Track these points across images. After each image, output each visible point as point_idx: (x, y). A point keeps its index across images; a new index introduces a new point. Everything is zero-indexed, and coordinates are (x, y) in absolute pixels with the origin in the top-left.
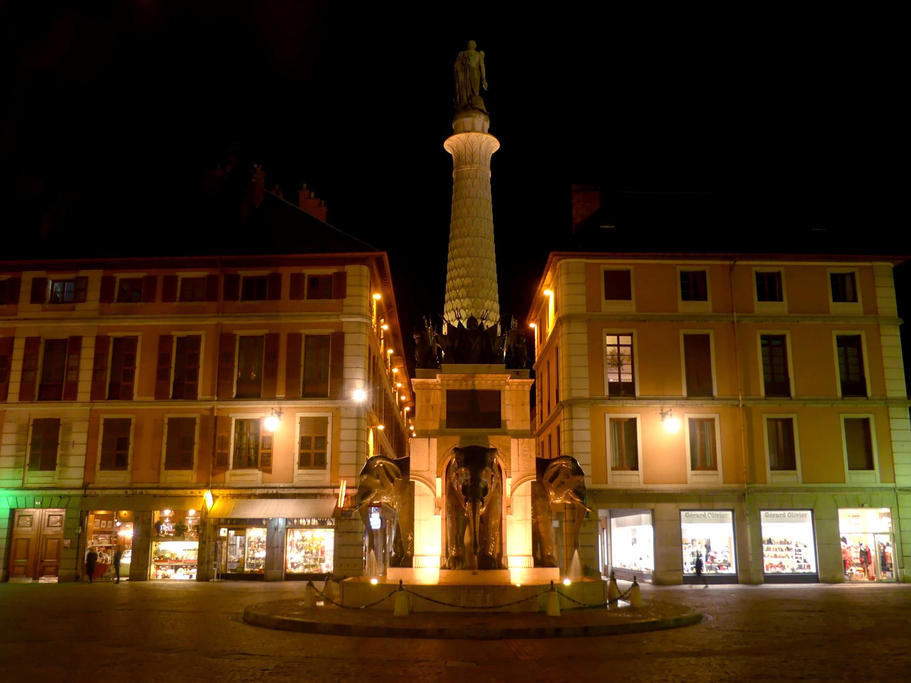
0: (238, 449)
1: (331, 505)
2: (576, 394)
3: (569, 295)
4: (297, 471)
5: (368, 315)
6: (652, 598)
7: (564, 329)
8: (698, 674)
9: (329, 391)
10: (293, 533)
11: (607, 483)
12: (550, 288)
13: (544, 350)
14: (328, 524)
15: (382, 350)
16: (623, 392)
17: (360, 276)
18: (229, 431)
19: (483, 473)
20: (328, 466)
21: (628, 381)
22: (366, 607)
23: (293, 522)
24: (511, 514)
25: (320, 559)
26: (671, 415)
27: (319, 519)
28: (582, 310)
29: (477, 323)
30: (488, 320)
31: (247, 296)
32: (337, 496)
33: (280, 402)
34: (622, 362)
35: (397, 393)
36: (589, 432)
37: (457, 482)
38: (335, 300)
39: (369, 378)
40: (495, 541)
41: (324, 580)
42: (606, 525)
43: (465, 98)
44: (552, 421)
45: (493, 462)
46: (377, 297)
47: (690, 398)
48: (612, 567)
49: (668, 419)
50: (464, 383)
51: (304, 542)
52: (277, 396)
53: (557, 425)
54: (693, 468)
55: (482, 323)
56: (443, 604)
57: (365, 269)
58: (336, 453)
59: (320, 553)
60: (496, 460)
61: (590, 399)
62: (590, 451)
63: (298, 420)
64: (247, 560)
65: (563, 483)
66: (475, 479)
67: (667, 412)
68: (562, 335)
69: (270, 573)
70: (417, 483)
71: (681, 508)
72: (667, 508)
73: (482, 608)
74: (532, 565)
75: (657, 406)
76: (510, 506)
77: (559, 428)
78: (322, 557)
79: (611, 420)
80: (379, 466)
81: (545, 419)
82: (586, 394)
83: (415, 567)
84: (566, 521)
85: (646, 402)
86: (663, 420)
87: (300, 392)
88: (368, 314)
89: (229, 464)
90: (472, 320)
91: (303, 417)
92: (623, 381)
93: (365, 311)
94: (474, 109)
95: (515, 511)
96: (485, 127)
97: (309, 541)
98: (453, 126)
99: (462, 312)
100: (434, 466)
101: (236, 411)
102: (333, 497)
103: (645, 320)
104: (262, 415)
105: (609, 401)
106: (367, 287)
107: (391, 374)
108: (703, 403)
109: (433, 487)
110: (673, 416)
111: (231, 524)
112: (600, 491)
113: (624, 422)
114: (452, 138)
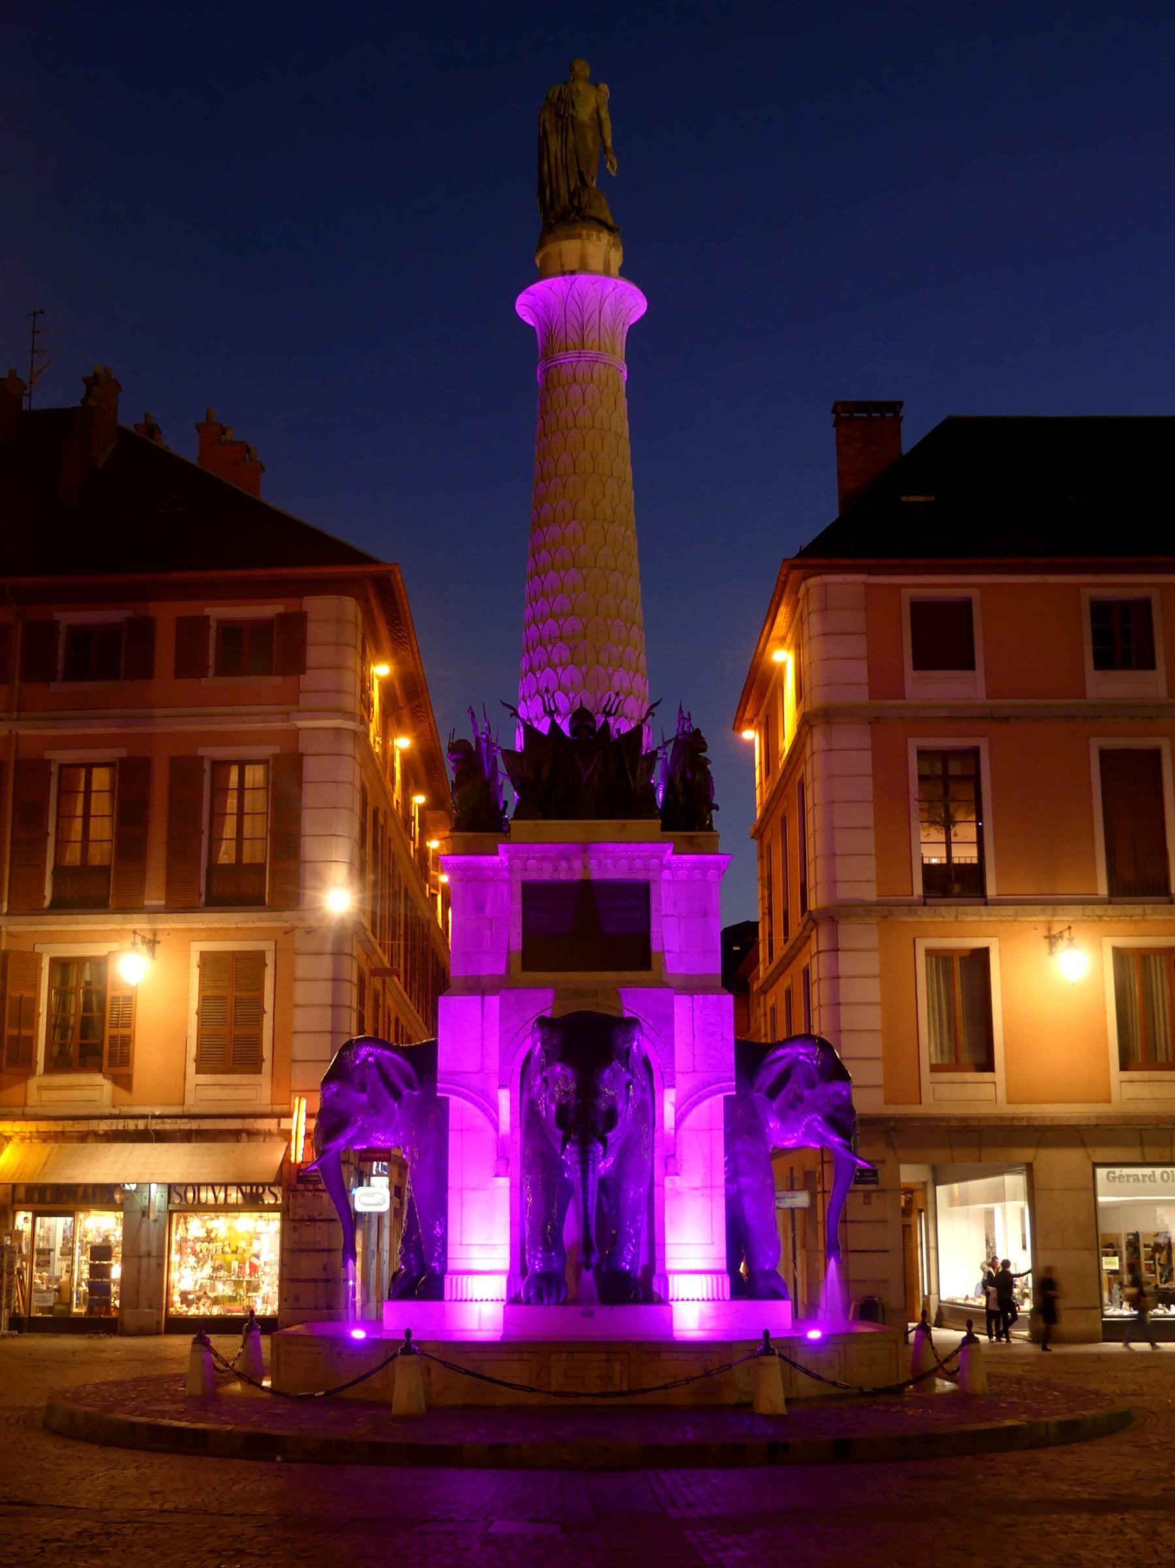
0: (58, 1025)
1: (269, 1158)
2: (845, 892)
3: (828, 659)
4: (194, 1079)
5: (358, 711)
6: (1020, 1372)
7: (817, 741)
8: (1083, 1553)
9: (267, 891)
10: (185, 1223)
11: (921, 1103)
12: (786, 646)
13: (775, 793)
14: (266, 1202)
15: (397, 795)
16: (957, 888)
17: (340, 621)
18: (36, 987)
19: (606, 1076)
20: (267, 1066)
21: (968, 861)
22: (327, 1393)
23: (184, 1197)
24: (677, 1174)
25: (249, 1282)
26: (1071, 940)
27: (243, 1188)
28: (860, 696)
29: (594, 722)
30: (620, 716)
31: (77, 671)
32: (287, 1135)
33: (152, 916)
34: (954, 817)
35: (439, 897)
36: (877, 982)
37: (545, 1099)
38: (280, 678)
39: (363, 864)
40: (637, 1235)
41: (240, 1333)
42: (926, 1202)
43: (564, 195)
44: (793, 959)
45: (628, 1050)
46: (382, 670)
47: (1114, 899)
48: (940, 1301)
49: (1062, 947)
50: (563, 864)
51: (211, 1244)
52: (147, 903)
53: (803, 965)
54: (1124, 1067)
55: (606, 724)
56: (510, 1386)
57: (350, 606)
58: (282, 1033)
59: (248, 1271)
60: (638, 1046)
61: (877, 904)
62: (878, 1026)
63: (195, 959)
64: (79, 1285)
65: (800, 1099)
66: (587, 1089)
67: (1061, 932)
68: (813, 754)
69: (130, 1320)
70: (455, 1101)
71: (1096, 1160)
72: (1070, 1158)
73: (600, 1395)
74: (727, 1297)
75: (1037, 919)
76: (673, 1156)
77: (807, 973)
78: (253, 1279)
79: (929, 952)
80: (365, 1061)
81: (778, 954)
82: (869, 893)
83: (450, 1300)
84: (824, 1192)
85: (1011, 910)
86: (1051, 953)
87: (200, 895)
88: (359, 709)
89: (37, 1063)
90: (581, 717)
91: (204, 952)
92: (956, 861)
93: (351, 703)
94: (584, 218)
95: (685, 1166)
96: (612, 262)
97: (223, 1241)
98: (538, 262)
99: (559, 696)
100: (493, 1064)
101: (53, 938)
102: (278, 1139)
103: (1007, 718)
104: (113, 946)
105: (926, 908)
106: (355, 647)
107: (423, 851)
108: (1147, 911)
109: (491, 1111)
110: (1074, 942)
111: (42, 1200)
112: (899, 1119)
113: (961, 958)
114: (537, 287)
